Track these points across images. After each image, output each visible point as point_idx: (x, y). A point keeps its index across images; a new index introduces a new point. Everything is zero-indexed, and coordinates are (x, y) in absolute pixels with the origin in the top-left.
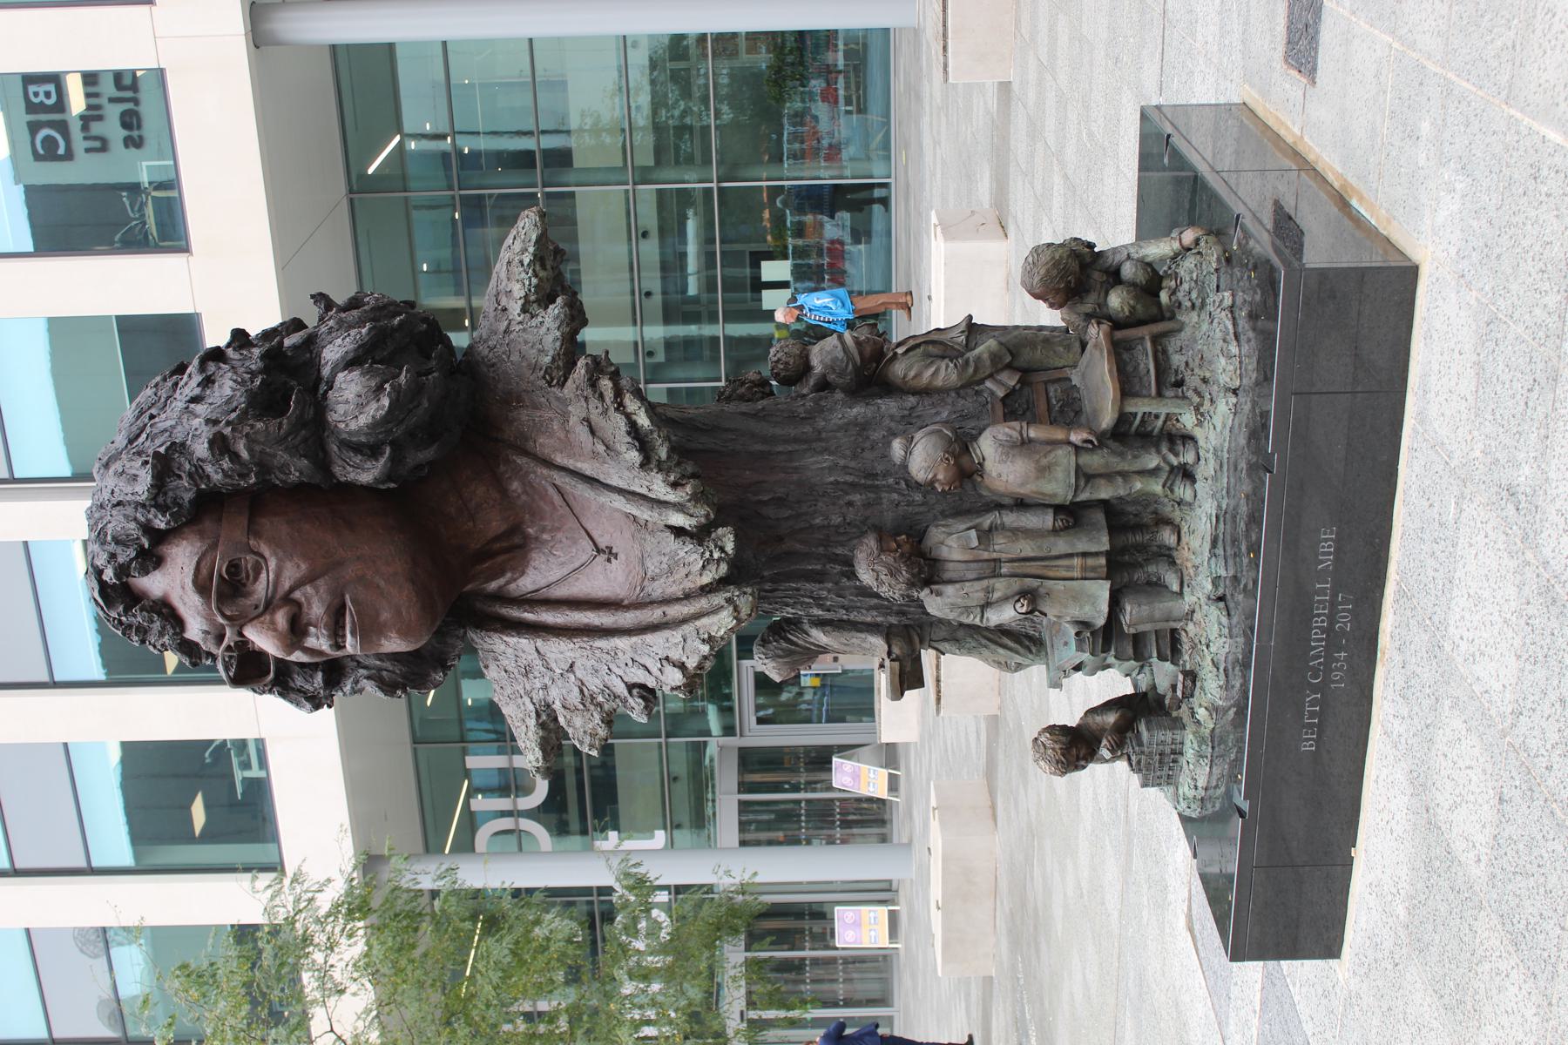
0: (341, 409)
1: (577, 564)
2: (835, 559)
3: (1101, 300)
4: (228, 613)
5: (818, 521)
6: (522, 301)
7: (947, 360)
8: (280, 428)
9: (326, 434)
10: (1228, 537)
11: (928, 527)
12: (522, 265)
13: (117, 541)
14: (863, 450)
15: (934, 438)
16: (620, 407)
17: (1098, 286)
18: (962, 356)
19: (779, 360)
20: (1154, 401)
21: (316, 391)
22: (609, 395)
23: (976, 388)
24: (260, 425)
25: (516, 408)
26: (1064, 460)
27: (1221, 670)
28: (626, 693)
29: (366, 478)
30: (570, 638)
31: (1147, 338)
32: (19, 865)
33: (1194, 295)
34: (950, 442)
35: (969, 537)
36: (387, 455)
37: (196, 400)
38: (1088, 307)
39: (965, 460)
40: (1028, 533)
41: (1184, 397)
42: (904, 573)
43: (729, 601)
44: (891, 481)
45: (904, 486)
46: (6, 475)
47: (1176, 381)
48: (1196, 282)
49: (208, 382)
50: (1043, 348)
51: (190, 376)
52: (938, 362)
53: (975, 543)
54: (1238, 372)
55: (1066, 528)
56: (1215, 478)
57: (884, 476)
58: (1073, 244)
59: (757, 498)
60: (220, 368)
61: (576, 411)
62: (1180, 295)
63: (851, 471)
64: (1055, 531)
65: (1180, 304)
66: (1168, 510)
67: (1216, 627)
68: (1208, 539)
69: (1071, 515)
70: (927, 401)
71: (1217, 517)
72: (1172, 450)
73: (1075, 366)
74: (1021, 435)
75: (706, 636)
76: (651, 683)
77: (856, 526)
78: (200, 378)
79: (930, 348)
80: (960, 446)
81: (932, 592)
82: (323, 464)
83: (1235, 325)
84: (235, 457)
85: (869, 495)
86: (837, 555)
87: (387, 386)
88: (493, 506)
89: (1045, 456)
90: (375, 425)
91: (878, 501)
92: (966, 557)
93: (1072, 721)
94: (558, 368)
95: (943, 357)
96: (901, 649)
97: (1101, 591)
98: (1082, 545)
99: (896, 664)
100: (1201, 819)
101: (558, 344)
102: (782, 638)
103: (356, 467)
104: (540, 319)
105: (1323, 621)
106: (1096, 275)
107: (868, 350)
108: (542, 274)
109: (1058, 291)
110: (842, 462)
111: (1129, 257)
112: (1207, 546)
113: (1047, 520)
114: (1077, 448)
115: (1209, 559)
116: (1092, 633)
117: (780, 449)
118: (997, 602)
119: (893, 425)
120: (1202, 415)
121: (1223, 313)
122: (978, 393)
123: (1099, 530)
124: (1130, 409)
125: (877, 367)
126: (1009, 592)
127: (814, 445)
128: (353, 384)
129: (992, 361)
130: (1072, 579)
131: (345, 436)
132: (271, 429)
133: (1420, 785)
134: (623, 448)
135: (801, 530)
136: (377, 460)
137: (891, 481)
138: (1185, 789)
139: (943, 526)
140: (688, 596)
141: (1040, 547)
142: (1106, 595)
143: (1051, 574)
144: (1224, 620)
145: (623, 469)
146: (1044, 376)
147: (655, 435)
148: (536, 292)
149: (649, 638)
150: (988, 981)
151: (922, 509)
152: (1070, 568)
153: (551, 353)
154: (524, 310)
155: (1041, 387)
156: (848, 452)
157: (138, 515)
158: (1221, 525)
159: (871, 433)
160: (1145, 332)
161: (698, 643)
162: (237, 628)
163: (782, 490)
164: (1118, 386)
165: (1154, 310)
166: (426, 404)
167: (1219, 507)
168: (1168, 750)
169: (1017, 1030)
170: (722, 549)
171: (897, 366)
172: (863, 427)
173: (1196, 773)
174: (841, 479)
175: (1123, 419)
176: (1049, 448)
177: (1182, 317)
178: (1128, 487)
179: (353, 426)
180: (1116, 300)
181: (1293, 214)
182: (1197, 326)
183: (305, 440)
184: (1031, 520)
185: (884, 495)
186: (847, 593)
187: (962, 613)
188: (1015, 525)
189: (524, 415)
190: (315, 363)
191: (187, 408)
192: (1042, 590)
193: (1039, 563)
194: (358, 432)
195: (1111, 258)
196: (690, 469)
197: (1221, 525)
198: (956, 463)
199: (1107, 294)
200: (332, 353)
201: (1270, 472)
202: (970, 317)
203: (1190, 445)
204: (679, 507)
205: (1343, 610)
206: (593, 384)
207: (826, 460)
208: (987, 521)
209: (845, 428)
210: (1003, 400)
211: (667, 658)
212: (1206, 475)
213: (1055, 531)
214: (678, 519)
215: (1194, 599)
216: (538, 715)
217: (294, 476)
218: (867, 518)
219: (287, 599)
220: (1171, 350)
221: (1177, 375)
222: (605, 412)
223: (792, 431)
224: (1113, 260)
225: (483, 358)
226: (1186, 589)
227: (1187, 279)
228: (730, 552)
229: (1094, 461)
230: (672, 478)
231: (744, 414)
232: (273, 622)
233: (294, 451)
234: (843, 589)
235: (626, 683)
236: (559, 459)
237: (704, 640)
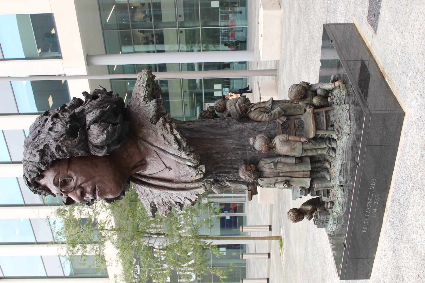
0: (92, 136)
1: (161, 170)
2: (233, 168)
3: (311, 100)
4: (63, 190)
5: (228, 158)
6: (143, 98)
7: (266, 113)
8: (75, 143)
9: (88, 143)
10: (345, 170)
11: (259, 160)
12: (143, 87)
13: (31, 171)
14: (241, 138)
15: (262, 139)
16: (172, 132)
17: (310, 96)
18: (270, 112)
19: (217, 106)
20: (325, 132)
21: (85, 130)
22: (169, 129)
24: (69, 142)
25: (142, 128)
26: (299, 146)
27: (341, 205)
28: (175, 204)
29: (100, 155)
30: (159, 189)
31: (324, 112)
32: (13, 160)
33: (338, 101)
34: (266, 140)
35: (271, 165)
36: (106, 149)
37: (50, 129)
38: (307, 102)
39: (270, 145)
41: (334, 130)
43: (204, 185)
46: (2, 58)
47: (332, 125)
48: (339, 98)
49: (54, 124)
50: (293, 109)
51: (49, 122)
52: (263, 114)
53: (273, 167)
54: (350, 130)
56: (342, 155)
57: (247, 146)
58: (303, 84)
59: (211, 152)
60: (57, 120)
61: (160, 132)
62: (334, 101)
63: (238, 144)
64: (296, 164)
65: (334, 103)
66: (328, 158)
67: (340, 195)
68: (339, 170)
69: (300, 160)
70: (260, 124)
71: (342, 165)
72: (330, 144)
73: (302, 114)
74: (287, 139)
75: (197, 194)
76: (182, 203)
77: (239, 160)
78: (52, 123)
79: (261, 109)
80: (270, 139)
82: (88, 151)
83: (350, 115)
84: (63, 151)
85: (243, 151)
87: (105, 131)
88: (137, 154)
89: (293, 145)
90: (102, 142)
91: (246, 153)
92: (270, 171)
93: (298, 207)
94: (154, 119)
95: (265, 112)
96: (251, 188)
97: (308, 181)
98: (303, 169)
99: (250, 192)
100: (334, 236)
101: (154, 113)
102: (218, 183)
103: (97, 152)
104: (149, 105)
105: (371, 201)
106: (310, 93)
107: (243, 109)
108: (149, 89)
109: (298, 99)
110: (235, 142)
111: (319, 88)
112: (338, 172)
113: (294, 161)
114: (302, 143)
115: (339, 176)
116: (305, 190)
117: (218, 137)
119: (250, 131)
120: (339, 138)
121: (346, 111)
122: (274, 122)
123: (308, 164)
124: (318, 134)
125: (246, 113)
126: (282, 180)
127: (228, 136)
128: (95, 129)
129: (279, 114)
131: (94, 144)
132: (73, 143)
133: (395, 252)
134: (173, 144)
135: (224, 160)
136: (103, 150)
137: (249, 148)
138: (329, 229)
139: (264, 161)
140: (192, 182)
141: (291, 169)
142: (310, 182)
143: (294, 176)
144: (342, 193)
145: (174, 148)
146: (293, 117)
147: (182, 140)
148: (147, 95)
149: (181, 192)
150: (272, 206)
151: (258, 155)
152: (299, 175)
153: (152, 115)
154: (144, 100)
155: (293, 121)
156: (237, 139)
157: (36, 165)
158: (343, 167)
159: (244, 133)
160: (323, 110)
161: (195, 195)
162: (66, 195)
163: (219, 150)
164: (315, 127)
165: (326, 103)
166: (116, 135)
167: (343, 163)
168: (325, 220)
169: (279, 222)
170: (201, 171)
171: (251, 114)
172: (242, 131)
173: (332, 226)
174: (235, 147)
175: (316, 135)
176: (295, 143)
177: (334, 106)
179: (96, 142)
180: (315, 101)
181: (367, 66)
182: (338, 110)
183: (83, 146)
184: (289, 161)
185: (247, 151)
186: (236, 176)
188: (284, 162)
189: (145, 130)
190: (84, 118)
191: (48, 132)
192: (291, 180)
194: (98, 143)
195: (314, 88)
196: (192, 149)
197: (343, 167)
198: (268, 146)
199: (312, 98)
200: (90, 117)
201: (358, 165)
202: (273, 99)
203: (335, 142)
204: (190, 161)
205: (377, 199)
206: (164, 126)
207: (231, 141)
208: (277, 160)
209: (236, 131)
210: (282, 125)
211: (186, 198)
212: (339, 153)
213: (296, 164)
214: (189, 164)
216: (151, 205)
217: (80, 155)
218: (242, 157)
219: (80, 187)
220: (330, 115)
221: (332, 123)
222: (168, 134)
223: (221, 132)
224: (314, 88)
225: (133, 112)
226: (332, 180)
227: (336, 96)
228: (204, 172)
229: (307, 146)
230: (187, 153)
231: (207, 126)
232: (76, 193)
233: (79, 149)
235: (175, 202)
236: (155, 144)
237: (196, 195)
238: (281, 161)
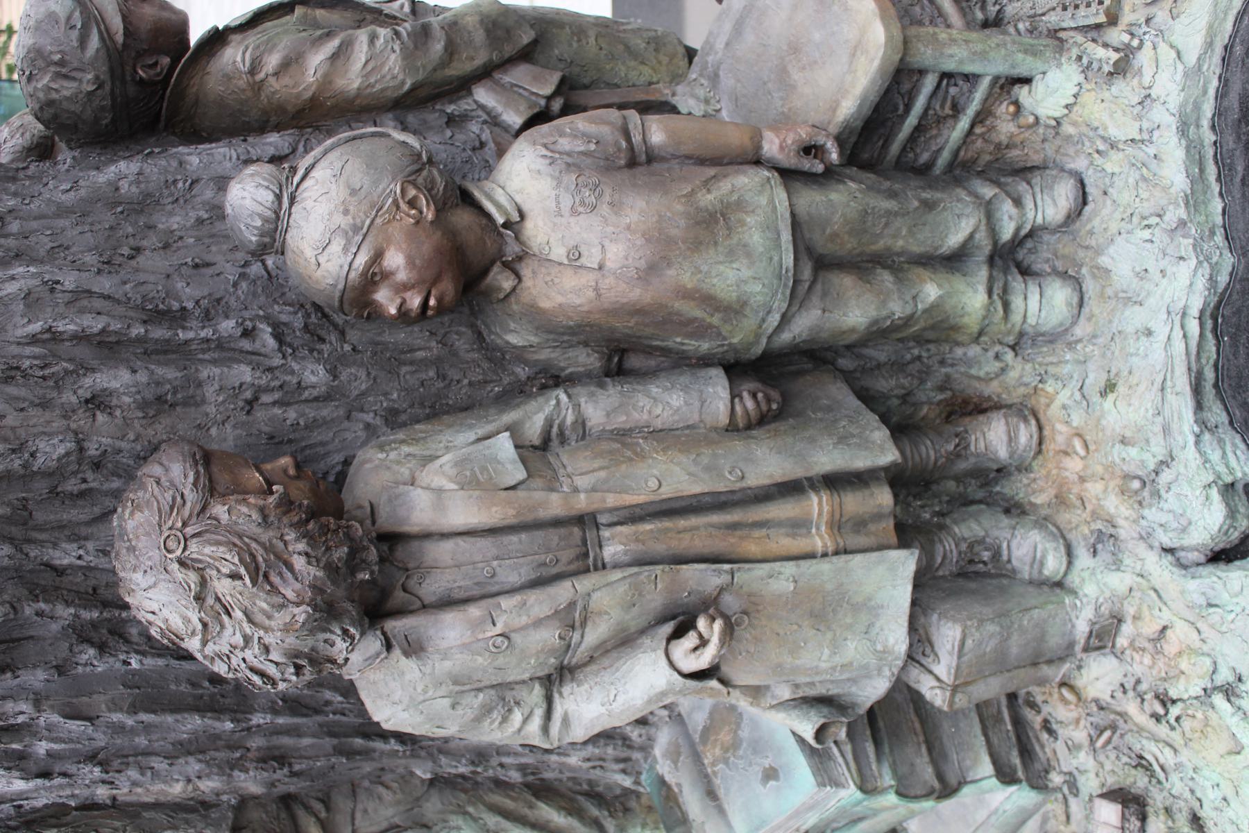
23: (450, 109)
40: (664, 437)
42: (299, 563)
44: (228, 326)
45: (271, 342)
55: (762, 420)
81: (389, 646)
85: (160, 371)
86: (59, 571)
118: (585, 665)
126: (634, 619)
130: (810, 556)
137: (228, 326)
142: (902, 595)
156: (90, 259)
174: (66, 327)
176: (711, 171)
178: (908, 298)
186: (99, 702)
187: (487, 710)
193: (715, 518)
215: (1118, 582)
234: (86, 686)
238: (581, 423)
